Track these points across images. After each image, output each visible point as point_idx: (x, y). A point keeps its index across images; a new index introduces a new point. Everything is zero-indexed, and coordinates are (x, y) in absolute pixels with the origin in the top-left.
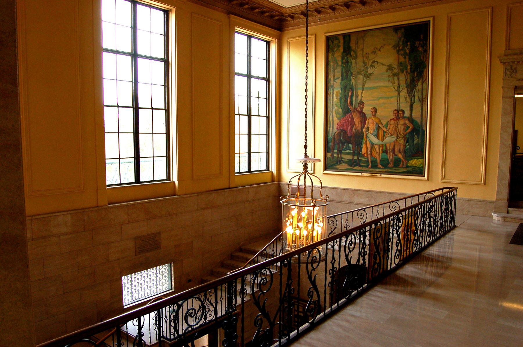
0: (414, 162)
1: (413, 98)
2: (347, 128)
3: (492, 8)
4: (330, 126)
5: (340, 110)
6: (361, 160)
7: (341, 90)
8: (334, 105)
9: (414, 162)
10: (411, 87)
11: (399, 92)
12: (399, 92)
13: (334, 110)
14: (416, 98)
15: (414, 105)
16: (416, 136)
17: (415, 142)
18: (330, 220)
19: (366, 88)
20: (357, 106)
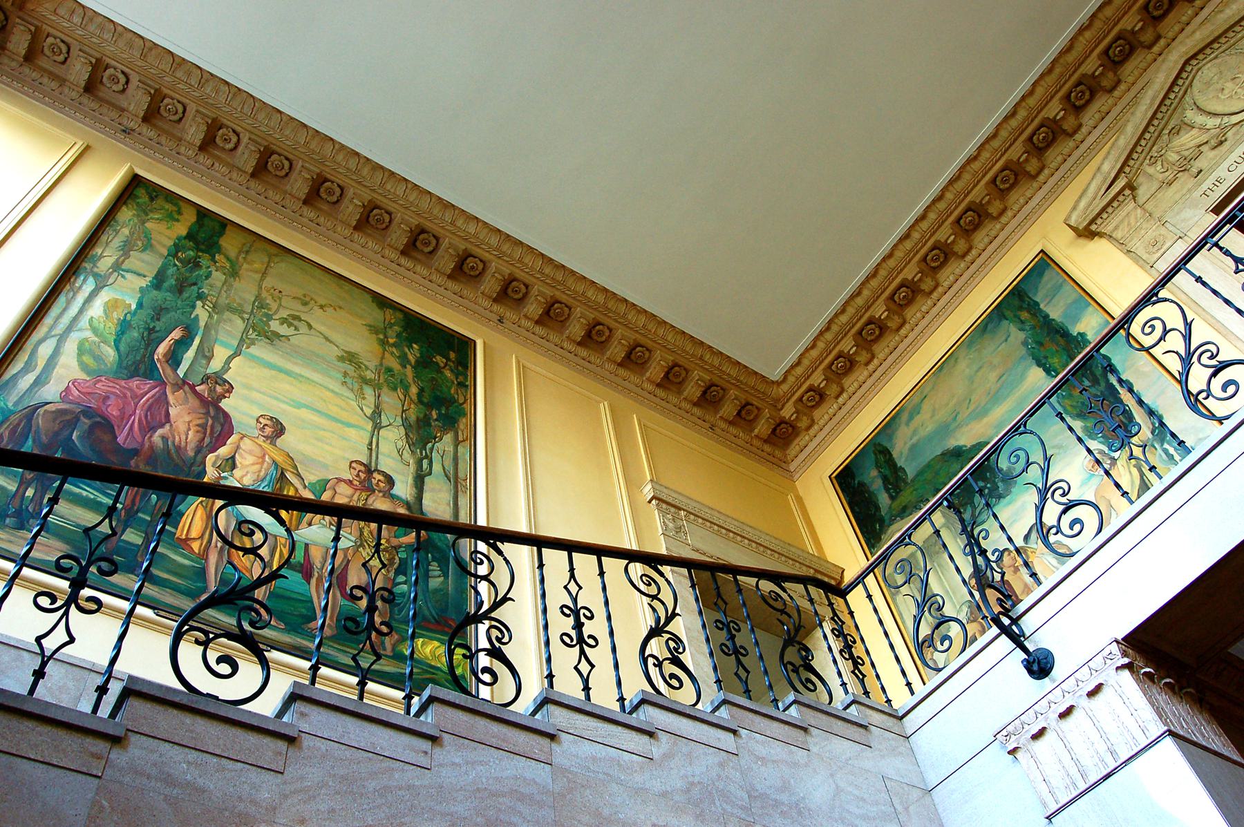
0: (428, 650)
1: (425, 462)
2: (124, 417)
3: (100, 777)
4: (27, 369)
5: (110, 353)
6: (163, 555)
7: (140, 305)
8: (84, 322)
9: (428, 650)
10: (421, 435)
11: (377, 427)
12: (377, 427)
13: (75, 337)
14: (437, 467)
15: (427, 479)
16: (434, 566)
17: (435, 583)
18: (170, 516)
19: (250, 354)
20: (198, 380)
